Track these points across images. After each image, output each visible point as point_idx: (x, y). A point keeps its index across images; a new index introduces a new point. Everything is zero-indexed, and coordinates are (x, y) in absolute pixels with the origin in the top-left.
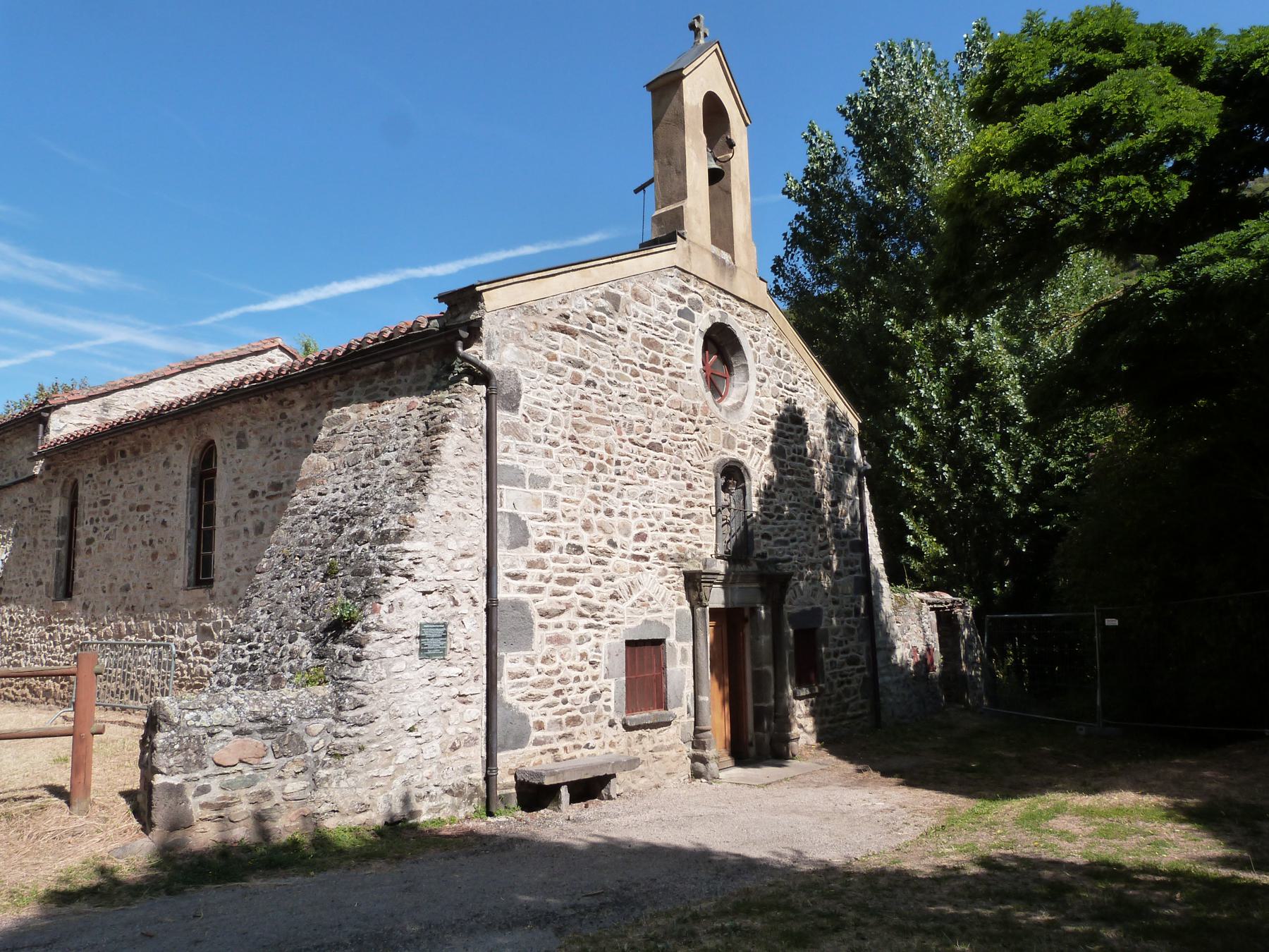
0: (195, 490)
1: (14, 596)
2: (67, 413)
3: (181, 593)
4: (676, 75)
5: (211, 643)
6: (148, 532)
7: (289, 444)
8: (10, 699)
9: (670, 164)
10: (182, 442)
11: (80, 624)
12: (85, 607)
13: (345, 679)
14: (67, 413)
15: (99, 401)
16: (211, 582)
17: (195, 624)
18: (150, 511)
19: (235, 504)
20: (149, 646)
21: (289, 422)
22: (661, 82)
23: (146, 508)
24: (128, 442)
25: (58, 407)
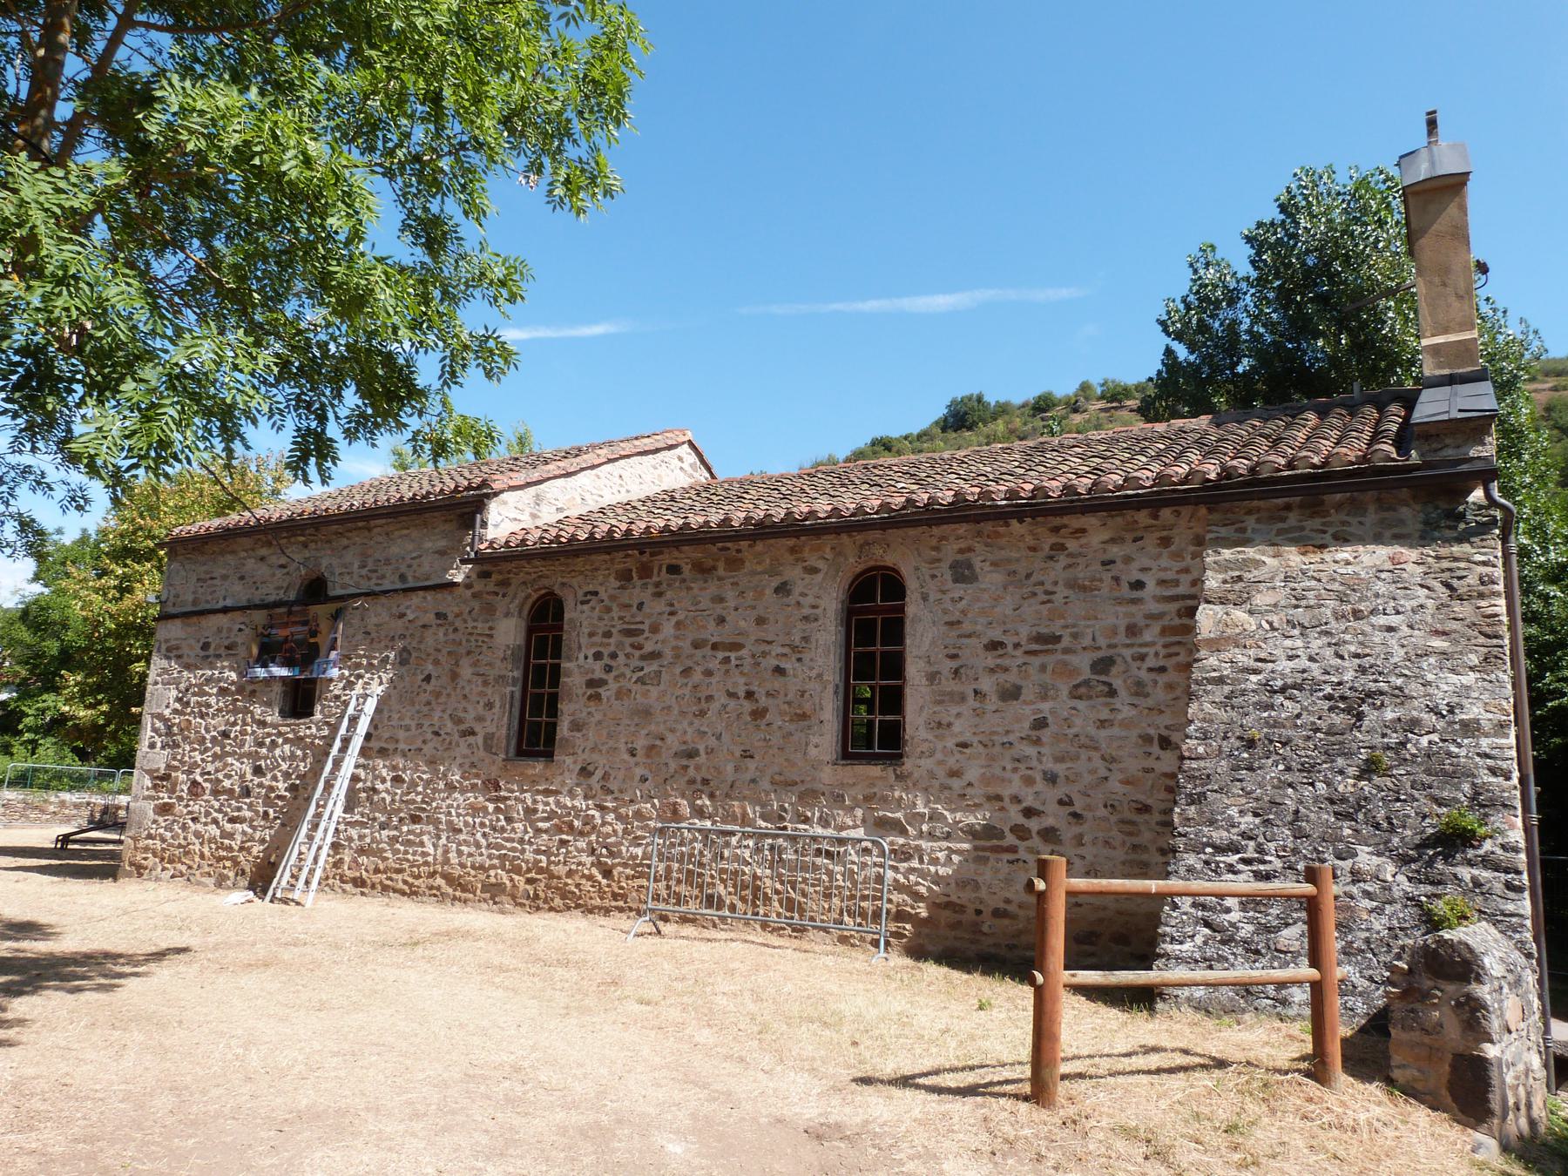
0: (842, 629)
1: (402, 746)
2: (505, 503)
3: (828, 769)
4: (1457, 179)
5: (901, 841)
6: (742, 680)
7: (1072, 585)
8: (403, 893)
9: (1444, 284)
10: (813, 561)
11: (572, 795)
12: (585, 772)
13: (1512, 915)
14: (505, 503)
15: (532, 490)
16: (901, 756)
17: (859, 812)
18: (744, 652)
19: (954, 657)
20: (745, 836)
21: (1070, 555)
22: (1428, 185)
23: (736, 647)
24: (685, 557)
25: (496, 494)
